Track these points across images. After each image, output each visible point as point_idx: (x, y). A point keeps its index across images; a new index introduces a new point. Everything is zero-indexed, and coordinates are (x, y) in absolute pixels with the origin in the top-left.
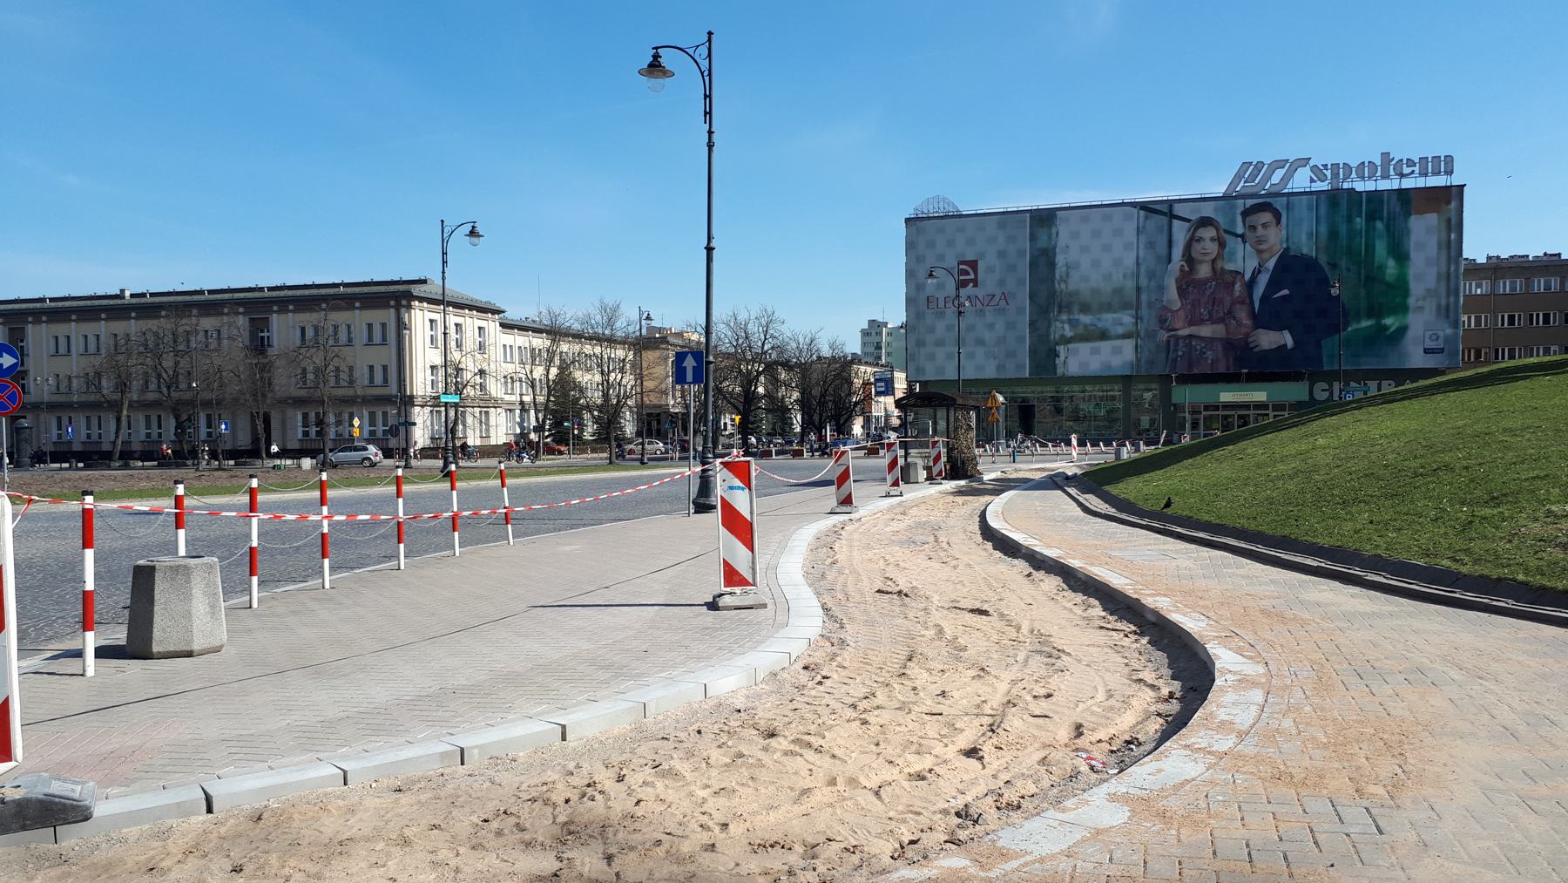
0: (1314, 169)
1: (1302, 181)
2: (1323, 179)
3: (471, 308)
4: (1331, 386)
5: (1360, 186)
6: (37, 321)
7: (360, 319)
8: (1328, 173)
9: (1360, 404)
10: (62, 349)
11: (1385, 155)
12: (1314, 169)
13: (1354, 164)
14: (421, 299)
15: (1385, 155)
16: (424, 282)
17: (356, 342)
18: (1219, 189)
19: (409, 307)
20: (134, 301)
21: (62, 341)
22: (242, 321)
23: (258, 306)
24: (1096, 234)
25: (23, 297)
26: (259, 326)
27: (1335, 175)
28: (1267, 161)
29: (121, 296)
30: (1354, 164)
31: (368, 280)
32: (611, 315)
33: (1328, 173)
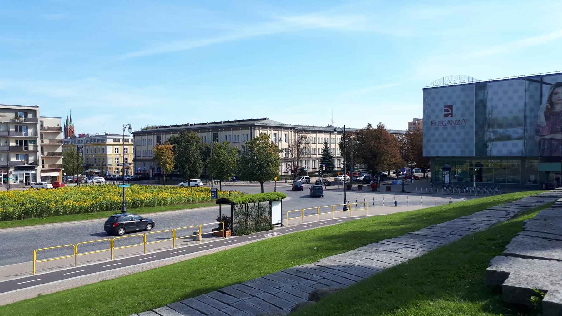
10: (237, 140)
16: (265, 119)
22: (155, 137)
23: (215, 128)
31: (213, 122)
32: (369, 125)
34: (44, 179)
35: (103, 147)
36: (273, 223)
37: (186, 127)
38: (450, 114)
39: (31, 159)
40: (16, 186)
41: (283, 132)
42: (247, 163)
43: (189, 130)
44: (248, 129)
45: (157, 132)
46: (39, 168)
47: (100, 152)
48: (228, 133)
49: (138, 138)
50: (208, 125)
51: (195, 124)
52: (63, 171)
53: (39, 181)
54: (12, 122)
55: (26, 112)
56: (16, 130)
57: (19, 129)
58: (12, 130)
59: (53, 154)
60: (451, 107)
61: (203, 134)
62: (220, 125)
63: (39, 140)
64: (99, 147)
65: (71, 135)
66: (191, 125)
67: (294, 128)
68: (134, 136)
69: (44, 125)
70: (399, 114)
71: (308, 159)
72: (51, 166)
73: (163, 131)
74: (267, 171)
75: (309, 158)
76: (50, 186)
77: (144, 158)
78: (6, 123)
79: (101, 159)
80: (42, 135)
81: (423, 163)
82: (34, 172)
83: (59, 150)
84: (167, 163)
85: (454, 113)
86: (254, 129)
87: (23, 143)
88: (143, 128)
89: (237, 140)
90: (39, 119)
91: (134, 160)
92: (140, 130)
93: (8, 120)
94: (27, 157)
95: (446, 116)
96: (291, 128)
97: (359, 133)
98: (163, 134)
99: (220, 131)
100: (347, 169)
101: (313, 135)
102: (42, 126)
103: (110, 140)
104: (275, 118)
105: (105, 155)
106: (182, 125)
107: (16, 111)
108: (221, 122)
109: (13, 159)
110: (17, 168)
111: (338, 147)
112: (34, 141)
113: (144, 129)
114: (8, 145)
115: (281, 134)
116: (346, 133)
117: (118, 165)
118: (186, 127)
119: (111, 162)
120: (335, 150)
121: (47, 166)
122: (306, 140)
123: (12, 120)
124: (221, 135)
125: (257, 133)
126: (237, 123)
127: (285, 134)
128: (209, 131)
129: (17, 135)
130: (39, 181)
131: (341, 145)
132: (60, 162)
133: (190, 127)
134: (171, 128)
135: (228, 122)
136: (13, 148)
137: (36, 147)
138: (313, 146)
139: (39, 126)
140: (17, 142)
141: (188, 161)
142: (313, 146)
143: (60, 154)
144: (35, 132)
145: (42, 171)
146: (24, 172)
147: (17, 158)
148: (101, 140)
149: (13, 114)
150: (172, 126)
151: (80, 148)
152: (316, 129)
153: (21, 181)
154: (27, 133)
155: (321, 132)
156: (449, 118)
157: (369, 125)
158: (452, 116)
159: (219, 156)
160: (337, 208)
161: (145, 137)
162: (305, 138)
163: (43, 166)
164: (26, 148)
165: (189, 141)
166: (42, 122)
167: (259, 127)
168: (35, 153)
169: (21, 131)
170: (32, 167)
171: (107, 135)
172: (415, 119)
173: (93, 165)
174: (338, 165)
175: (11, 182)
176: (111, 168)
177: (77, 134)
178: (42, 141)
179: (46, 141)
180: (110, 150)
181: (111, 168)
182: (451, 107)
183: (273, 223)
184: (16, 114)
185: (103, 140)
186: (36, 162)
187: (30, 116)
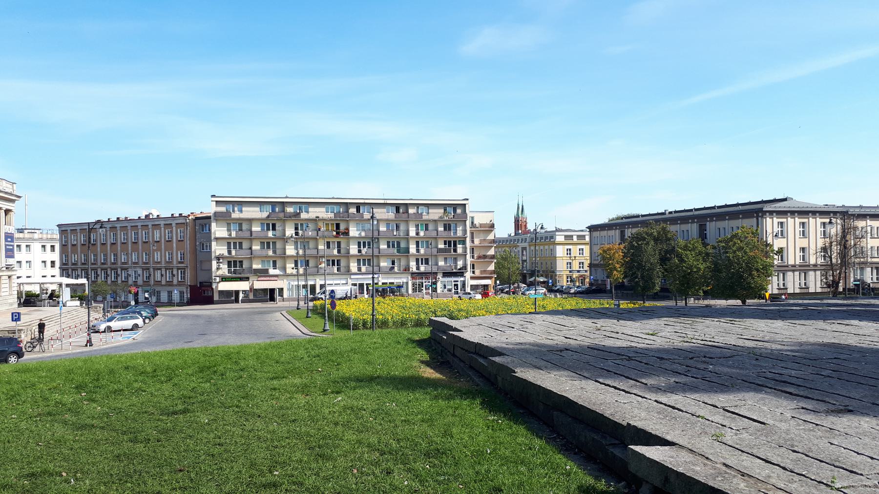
16: (785, 200)
34: (474, 288)
35: (551, 247)
39: (460, 264)
40: (445, 296)
42: (720, 271)
43: (665, 221)
44: (753, 217)
45: (620, 225)
46: (468, 274)
47: (548, 253)
48: (721, 224)
49: (596, 234)
50: (640, 219)
51: (676, 212)
52: (496, 279)
53: (468, 290)
54: (441, 219)
55: (455, 207)
56: (445, 229)
57: (447, 227)
58: (441, 229)
59: (485, 257)
61: (685, 227)
63: (468, 240)
64: (546, 247)
65: (523, 229)
66: (670, 213)
68: (590, 231)
69: (476, 222)
71: (863, 266)
72: (482, 272)
73: (628, 224)
74: (749, 283)
75: (865, 263)
76: (479, 297)
78: (435, 221)
79: (549, 263)
80: (472, 234)
82: (462, 279)
83: (492, 252)
84: (615, 269)
86: (762, 217)
87: (452, 244)
88: (611, 218)
90: (469, 215)
91: (590, 266)
92: (607, 221)
93: (436, 218)
94: (455, 260)
96: (835, 213)
99: (710, 221)
102: (472, 223)
103: (560, 238)
105: (554, 258)
106: (650, 215)
107: (445, 206)
108: (713, 208)
109: (441, 263)
110: (446, 274)
112: (463, 242)
113: (613, 220)
114: (437, 247)
117: (570, 272)
119: (561, 267)
121: (478, 273)
122: (857, 233)
123: (441, 217)
124: (712, 227)
128: (693, 222)
129: (446, 234)
130: (468, 290)
132: (492, 267)
133: (667, 216)
135: (726, 206)
136: (440, 251)
137: (465, 249)
139: (468, 223)
140: (445, 244)
141: (640, 267)
143: (493, 257)
144: (465, 231)
145: (472, 278)
146: (453, 279)
147: (446, 263)
148: (549, 239)
149: (442, 211)
151: (524, 249)
153: (450, 290)
154: (455, 233)
159: (682, 260)
161: (604, 233)
162: (855, 228)
163: (474, 272)
164: (455, 251)
165: (644, 239)
166: (473, 218)
167: (771, 213)
168: (464, 255)
169: (450, 229)
170: (460, 273)
171: (558, 230)
173: (538, 271)
175: (439, 291)
176: (561, 276)
177: (531, 227)
178: (473, 242)
179: (477, 241)
180: (560, 251)
181: (561, 276)
184: (445, 210)
185: (552, 237)
186: (465, 267)
187: (459, 211)
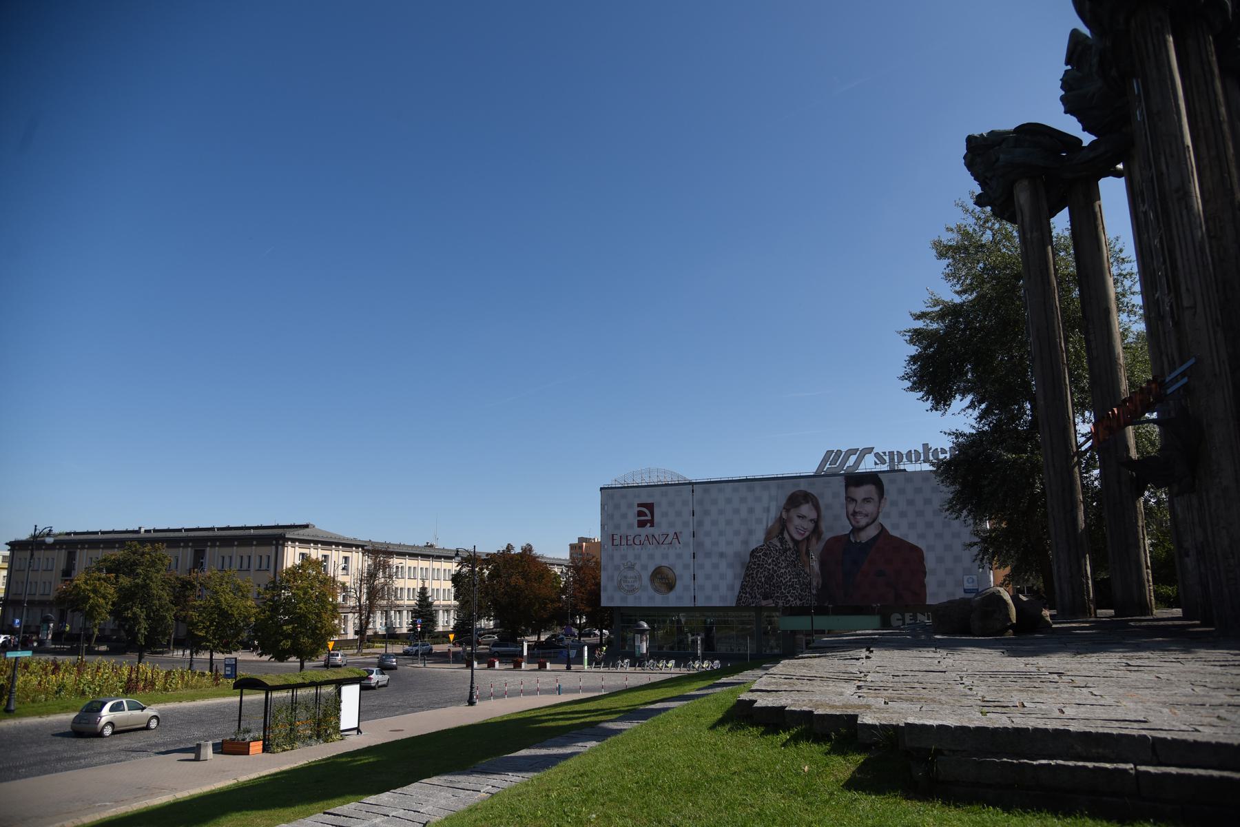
0: (877, 455)
1: (868, 465)
2: (883, 462)
3: (337, 544)
4: (903, 615)
5: (910, 468)
6: (213, 546)
7: (255, 551)
8: (887, 458)
9: (96, 765)
10: (264, 566)
11: (925, 446)
12: (877, 455)
13: (904, 452)
14: (293, 541)
15: (925, 446)
16: (307, 526)
17: (252, 569)
18: (810, 468)
19: (283, 546)
20: (148, 535)
21: (227, 560)
22: (189, 552)
23: (200, 542)
24: (729, 501)
25: (201, 526)
26: (71, 558)
27: (892, 460)
28: (844, 450)
29: (138, 532)
30: (904, 452)
31: (224, 526)
32: (509, 547)
33: (887, 458)
36: (342, 728)
37: (135, 536)
38: (647, 521)
41: (342, 554)
43: (143, 541)
44: (271, 544)
50: (184, 534)
51: (155, 531)
60: (650, 507)
62: (210, 533)
67: (362, 547)
70: (556, 526)
77: (45, 598)
81: (600, 616)
85: (656, 519)
89: (264, 566)
95: (642, 524)
97: (491, 559)
98: (83, 548)
100: (463, 631)
101: (409, 563)
104: (325, 525)
108: (212, 529)
111: (449, 585)
115: (336, 556)
116: (471, 559)
118: (135, 536)
120: (442, 591)
124: (213, 555)
125: (292, 556)
126: (247, 532)
127: (346, 559)
128: (186, 546)
131: (456, 579)
134: (100, 536)
138: (398, 583)
142: (398, 583)
150: (103, 533)
152: (404, 550)
155: (413, 556)
156: (648, 530)
157: (509, 547)
158: (652, 525)
160: (457, 702)
172: (581, 540)
174: (445, 622)
182: (650, 507)
183: (342, 728)
